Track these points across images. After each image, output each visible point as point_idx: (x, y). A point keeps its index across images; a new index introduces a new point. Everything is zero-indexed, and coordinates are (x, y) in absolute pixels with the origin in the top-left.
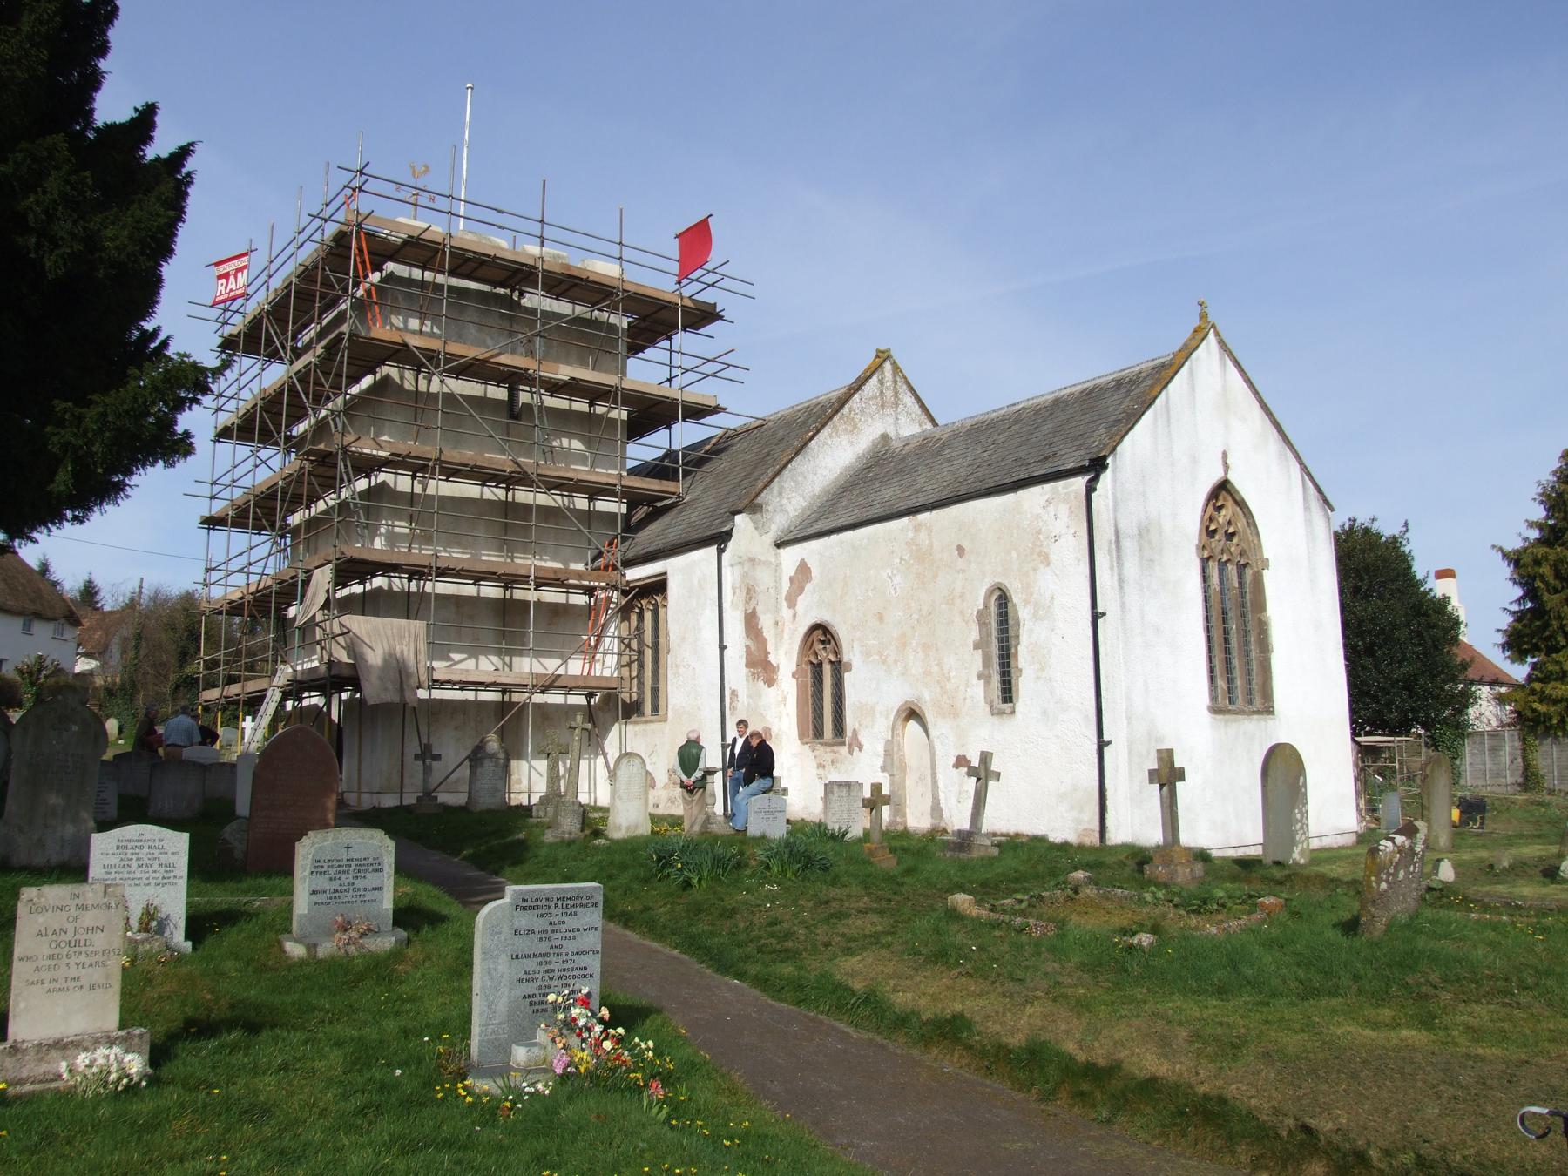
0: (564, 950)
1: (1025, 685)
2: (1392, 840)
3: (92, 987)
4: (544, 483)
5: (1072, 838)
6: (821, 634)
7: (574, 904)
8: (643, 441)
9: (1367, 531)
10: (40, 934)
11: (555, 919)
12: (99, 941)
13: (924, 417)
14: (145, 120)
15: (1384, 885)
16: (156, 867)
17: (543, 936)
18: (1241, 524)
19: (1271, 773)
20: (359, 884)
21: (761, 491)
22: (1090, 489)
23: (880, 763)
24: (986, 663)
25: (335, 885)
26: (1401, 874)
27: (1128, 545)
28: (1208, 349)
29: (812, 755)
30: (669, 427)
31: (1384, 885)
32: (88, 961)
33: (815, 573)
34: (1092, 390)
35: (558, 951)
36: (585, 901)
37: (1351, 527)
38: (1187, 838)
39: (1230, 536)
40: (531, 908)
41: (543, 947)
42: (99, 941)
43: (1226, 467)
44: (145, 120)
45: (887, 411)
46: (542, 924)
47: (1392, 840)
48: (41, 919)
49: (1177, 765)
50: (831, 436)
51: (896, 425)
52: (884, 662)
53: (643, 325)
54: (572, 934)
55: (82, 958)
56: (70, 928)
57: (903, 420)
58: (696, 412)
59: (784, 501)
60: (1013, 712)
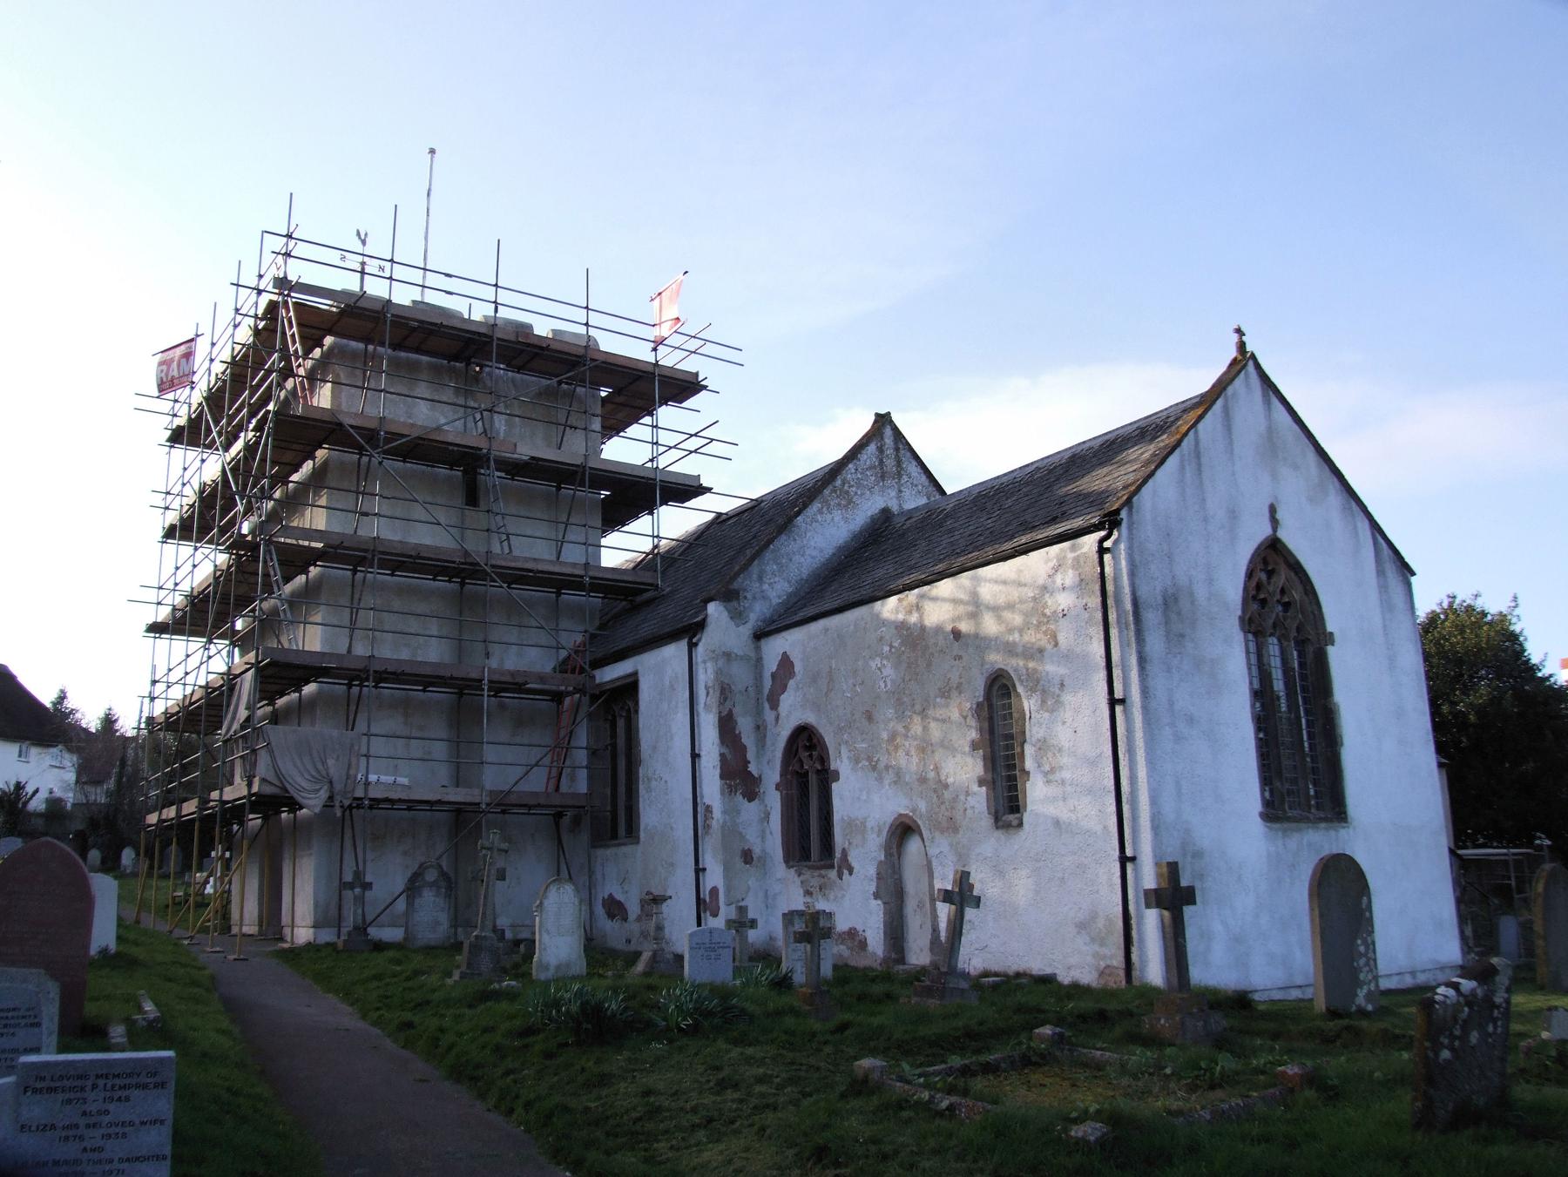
1: (1036, 792)
4: (500, 575)
5: (1087, 977)
6: (805, 741)
8: (625, 528)
9: (1470, 609)
13: (931, 489)
15: (1446, 1054)
18: (1297, 594)
21: (737, 574)
23: (873, 888)
26: (1474, 1037)
27: (1152, 618)
28: (1248, 385)
29: (798, 881)
30: (651, 513)
31: (1446, 1054)
33: (798, 667)
34: (1113, 442)
35: (95, 1156)
36: (143, 1079)
37: (1451, 605)
38: (1200, 975)
40: (51, 1090)
43: (1275, 522)
45: (888, 482)
49: (1184, 883)
50: (820, 511)
51: (899, 498)
52: (874, 768)
53: (621, 399)
57: (907, 493)
58: (684, 490)
59: (766, 587)
60: (1020, 825)
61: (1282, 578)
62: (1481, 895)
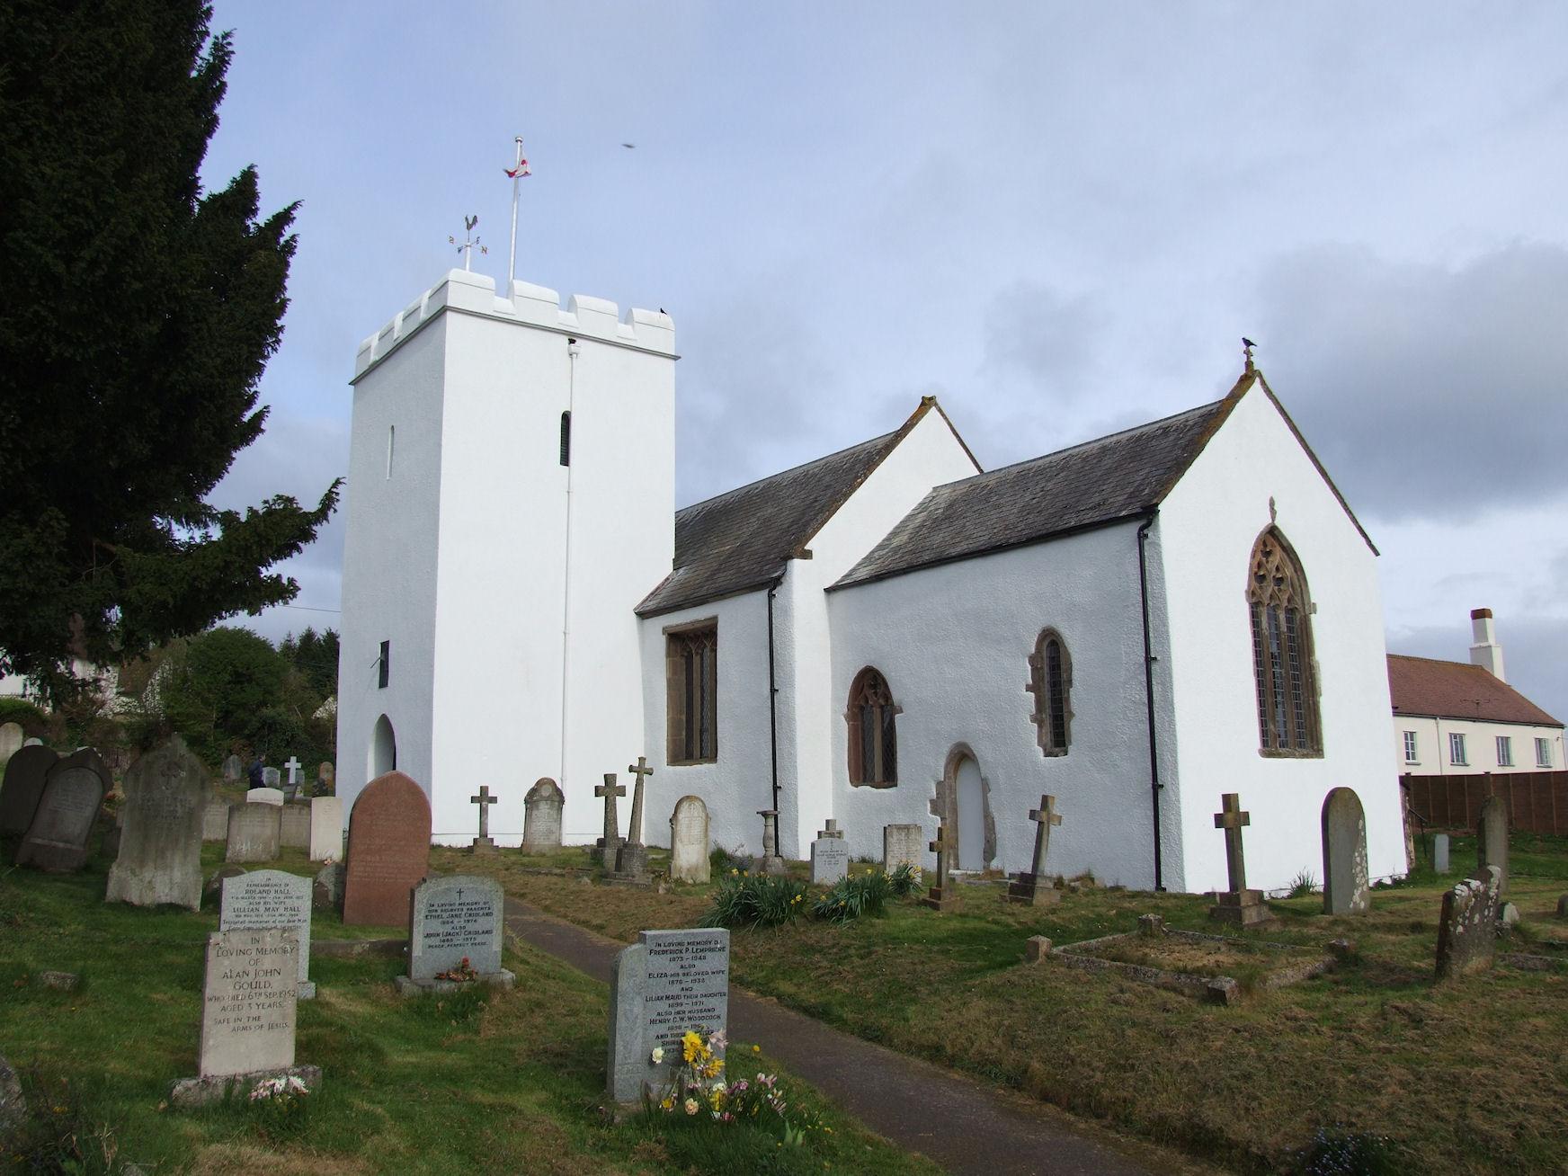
0: (694, 992)
1: (1075, 727)
2: (1468, 884)
3: (271, 1027)
7: (704, 947)
10: (225, 976)
11: (685, 963)
12: (277, 983)
14: (245, 188)
15: (1460, 929)
16: (281, 911)
17: (675, 979)
18: (1289, 571)
19: (1331, 818)
20: (470, 927)
22: (1142, 536)
24: (1038, 702)
25: (448, 928)
26: (1477, 918)
31: (1460, 929)
32: (267, 1002)
39: (1279, 581)
40: (664, 952)
41: (675, 990)
42: (277, 983)
43: (1273, 513)
44: (245, 188)
46: (673, 967)
47: (1468, 884)
48: (226, 962)
54: (701, 977)
55: (262, 999)
56: (251, 970)
61: (1278, 557)
62: (1420, 843)
